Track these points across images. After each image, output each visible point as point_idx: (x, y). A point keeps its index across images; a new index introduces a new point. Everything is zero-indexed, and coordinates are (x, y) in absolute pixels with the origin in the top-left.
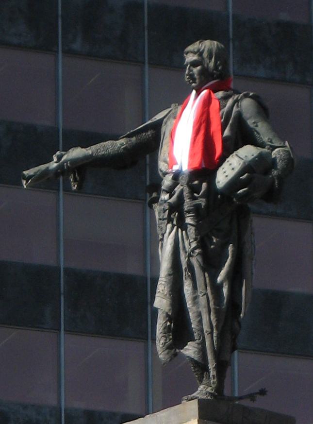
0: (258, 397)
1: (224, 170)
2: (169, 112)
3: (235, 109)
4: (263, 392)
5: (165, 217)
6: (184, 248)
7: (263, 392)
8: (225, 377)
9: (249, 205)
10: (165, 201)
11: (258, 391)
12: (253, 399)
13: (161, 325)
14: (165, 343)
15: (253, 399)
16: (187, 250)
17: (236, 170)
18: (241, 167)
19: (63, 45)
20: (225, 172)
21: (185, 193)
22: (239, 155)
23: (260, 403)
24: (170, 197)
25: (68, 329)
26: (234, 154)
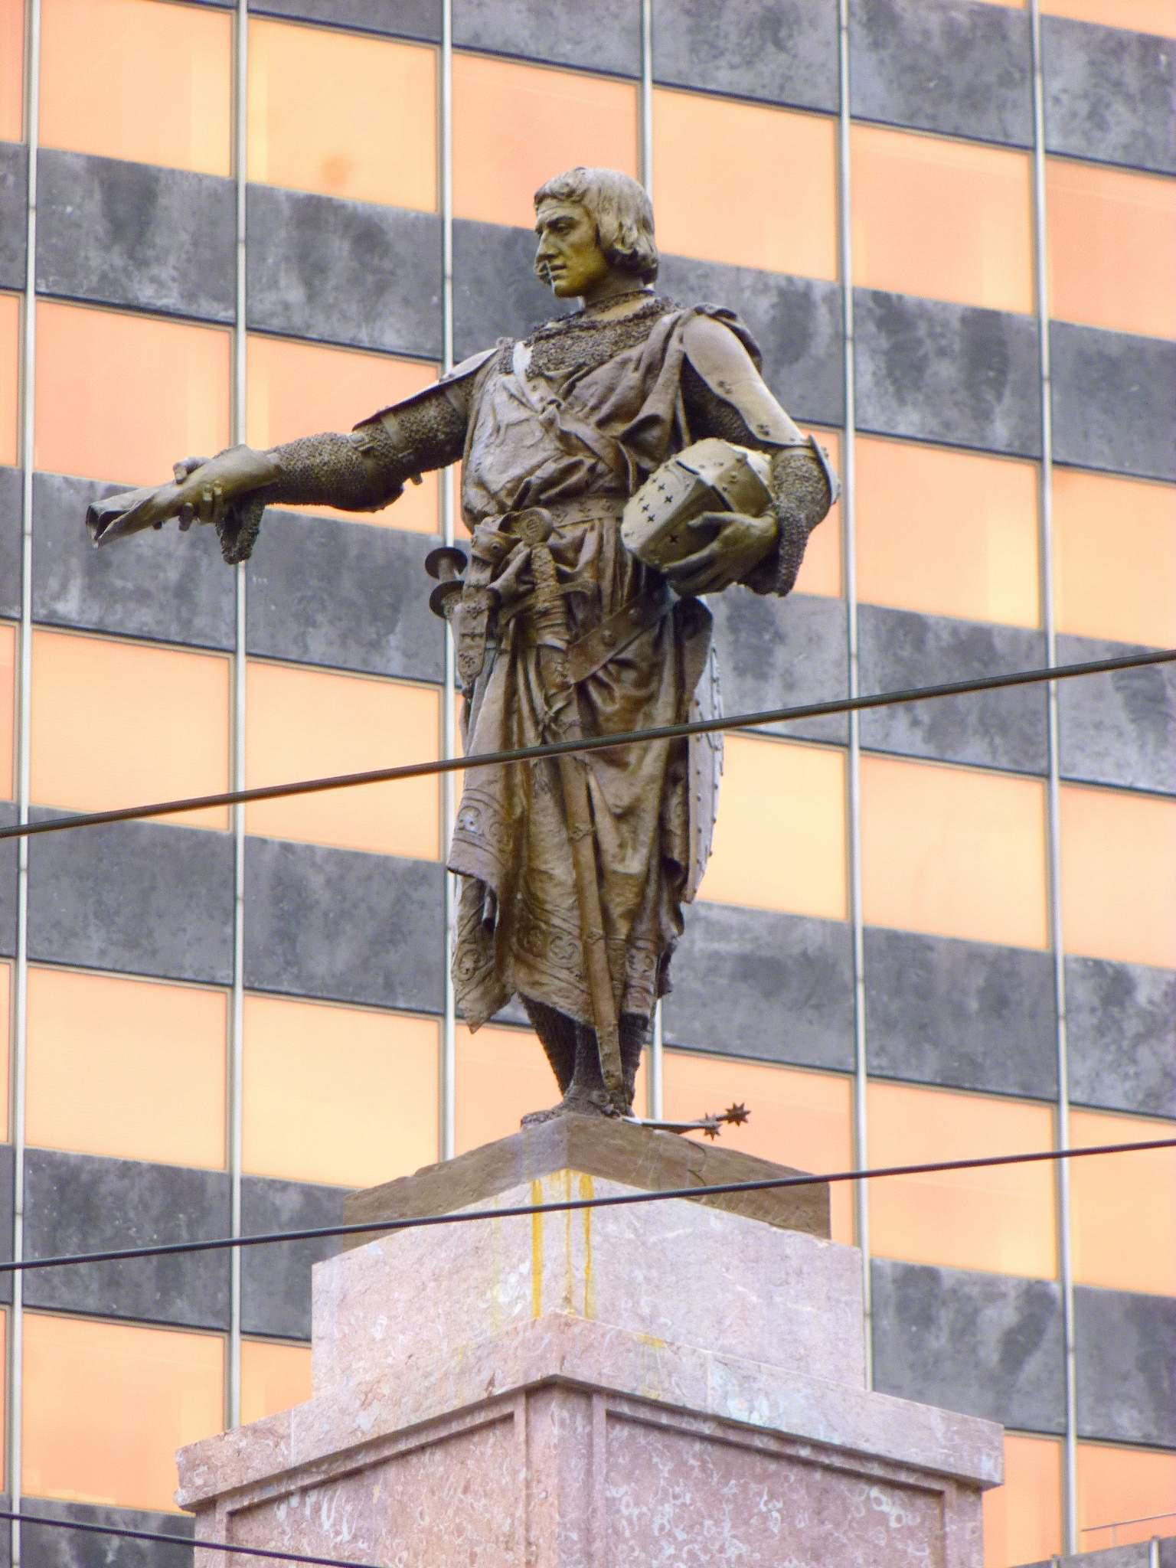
0: (725, 1127)
1: (644, 504)
2: (493, 355)
3: (674, 343)
4: (737, 1115)
5: (477, 631)
6: (533, 709)
7: (737, 1115)
8: (636, 1065)
9: (703, 598)
10: (478, 588)
11: (725, 1113)
12: (712, 1131)
13: (466, 921)
14: (475, 969)
15: (712, 1131)
16: (541, 716)
17: (679, 500)
18: (690, 495)
19: (663, 1029)
20: (645, 509)
21: (127, 495)
22: (685, 463)
23: (730, 1137)
24: (495, 577)
25: (32, 1302)
26: (671, 462)
